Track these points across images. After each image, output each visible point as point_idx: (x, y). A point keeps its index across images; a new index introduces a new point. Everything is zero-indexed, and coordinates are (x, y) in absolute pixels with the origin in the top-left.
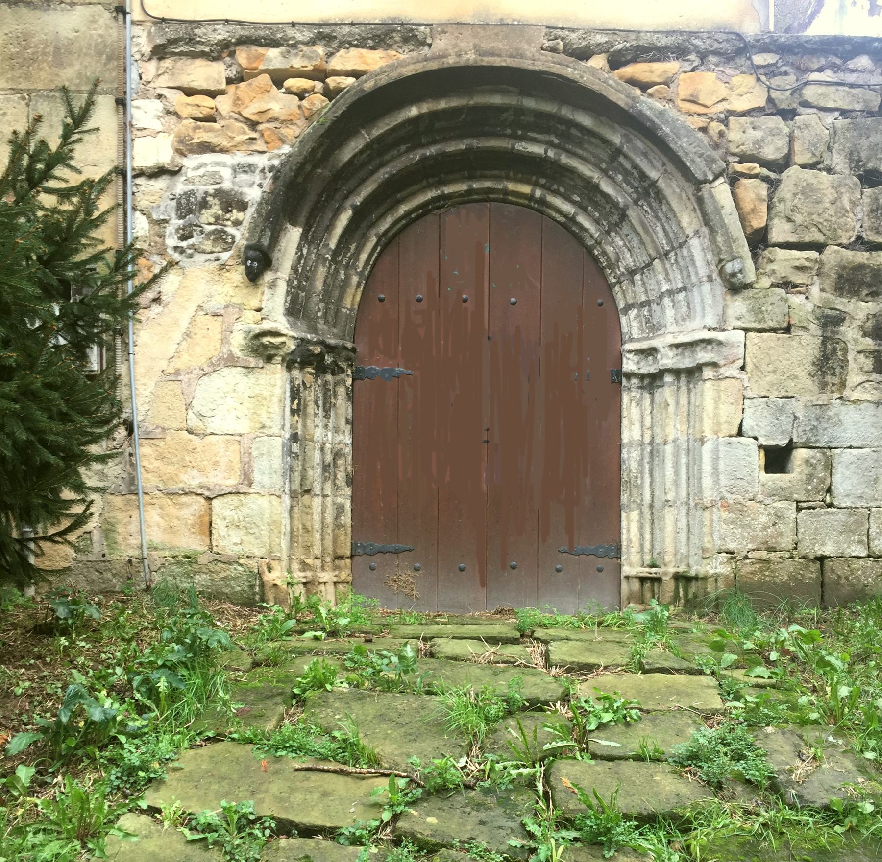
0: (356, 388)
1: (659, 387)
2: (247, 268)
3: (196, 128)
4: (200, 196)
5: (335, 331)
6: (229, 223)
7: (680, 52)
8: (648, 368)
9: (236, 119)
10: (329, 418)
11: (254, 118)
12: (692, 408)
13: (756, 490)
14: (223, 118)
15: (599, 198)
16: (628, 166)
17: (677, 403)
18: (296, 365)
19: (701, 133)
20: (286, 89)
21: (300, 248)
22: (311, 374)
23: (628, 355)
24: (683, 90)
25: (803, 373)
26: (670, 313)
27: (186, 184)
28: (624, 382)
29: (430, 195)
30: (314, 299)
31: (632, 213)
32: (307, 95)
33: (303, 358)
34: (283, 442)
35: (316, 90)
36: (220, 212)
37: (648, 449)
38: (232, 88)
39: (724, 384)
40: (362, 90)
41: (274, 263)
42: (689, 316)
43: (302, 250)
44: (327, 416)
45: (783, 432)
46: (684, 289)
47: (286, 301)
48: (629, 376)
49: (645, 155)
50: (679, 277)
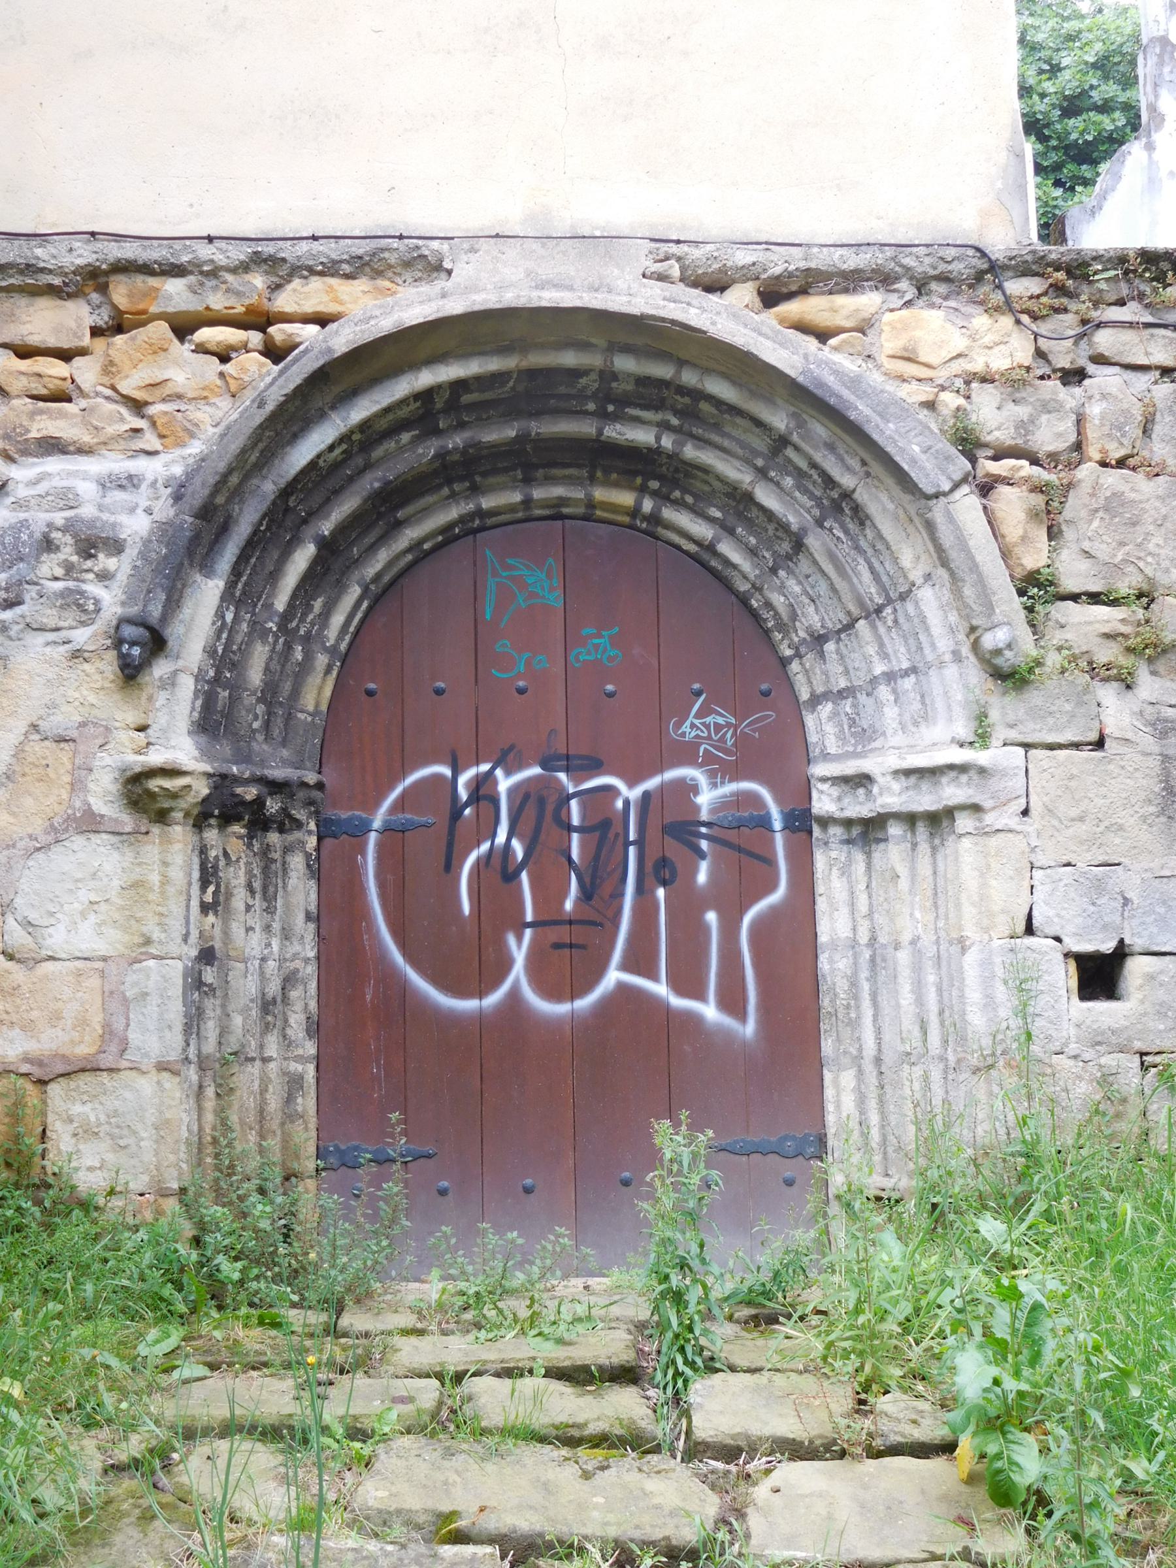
0: (324, 853)
1: (879, 841)
2: (122, 657)
3: (32, 415)
4: (39, 529)
5: (285, 753)
6: (91, 576)
7: (884, 279)
8: (858, 808)
9: (107, 398)
10: (273, 913)
11: (138, 395)
12: (941, 882)
13: (1065, 1034)
14: (83, 394)
15: (754, 513)
16: (803, 464)
17: (913, 870)
18: (213, 821)
19: (925, 412)
20: (197, 345)
21: (220, 614)
22: (240, 837)
23: (820, 786)
24: (887, 342)
25: (1132, 820)
26: (891, 713)
27: (14, 510)
28: (817, 831)
29: (453, 513)
30: (246, 702)
31: (813, 542)
32: (233, 355)
33: (224, 807)
34: (186, 967)
35: (250, 346)
36: (75, 558)
37: (867, 954)
38: (100, 344)
39: (994, 841)
40: (330, 350)
41: (170, 643)
42: (925, 718)
43: (223, 617)
44: (270, 910)
45: (1105, 927)
46: (914, 670)
47: (193, 709)
48: (825, 822)
49: (831, 447)
50: (903, 649)
